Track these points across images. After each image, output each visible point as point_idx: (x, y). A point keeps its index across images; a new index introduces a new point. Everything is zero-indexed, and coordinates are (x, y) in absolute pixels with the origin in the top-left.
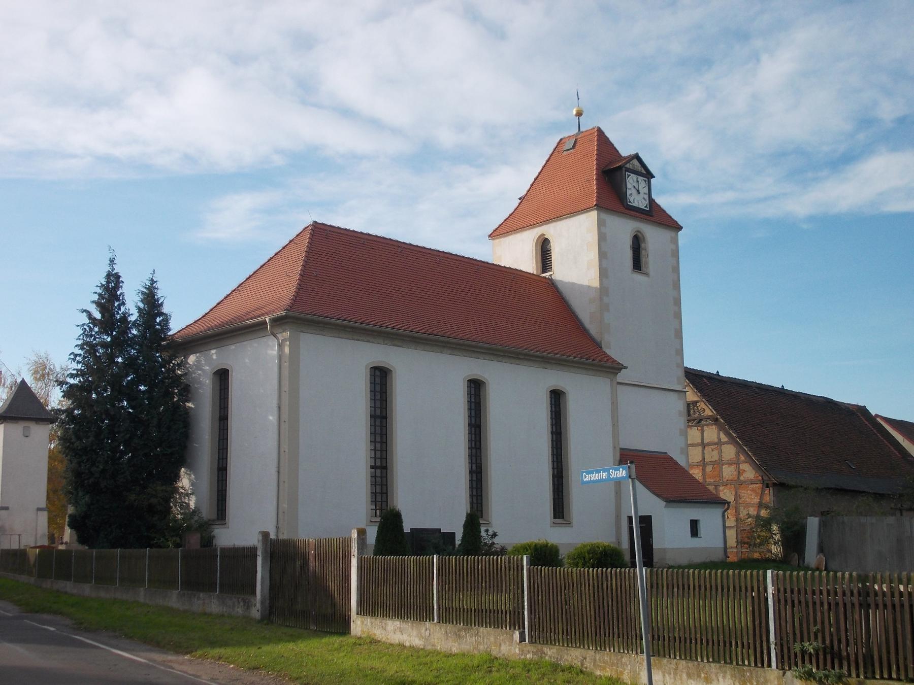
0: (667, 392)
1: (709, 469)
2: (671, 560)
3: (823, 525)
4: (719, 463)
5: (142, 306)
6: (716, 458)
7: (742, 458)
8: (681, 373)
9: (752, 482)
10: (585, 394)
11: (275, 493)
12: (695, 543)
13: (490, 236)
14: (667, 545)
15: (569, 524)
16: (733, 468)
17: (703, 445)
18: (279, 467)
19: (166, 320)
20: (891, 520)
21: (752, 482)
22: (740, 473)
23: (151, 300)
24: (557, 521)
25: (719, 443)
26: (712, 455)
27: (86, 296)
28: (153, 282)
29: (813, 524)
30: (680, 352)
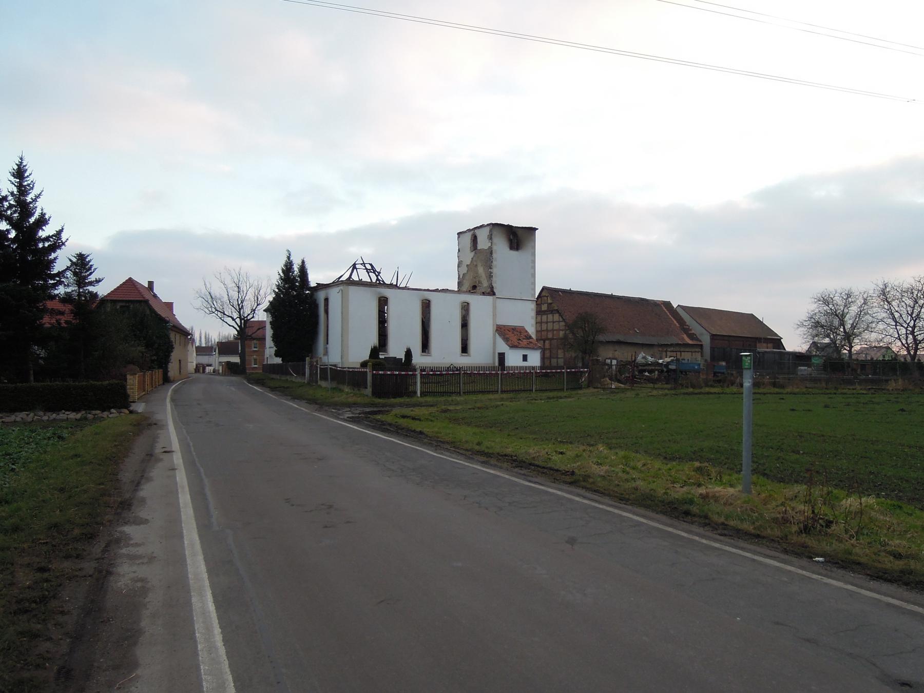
15: (469, 355)
28: (289, 258)
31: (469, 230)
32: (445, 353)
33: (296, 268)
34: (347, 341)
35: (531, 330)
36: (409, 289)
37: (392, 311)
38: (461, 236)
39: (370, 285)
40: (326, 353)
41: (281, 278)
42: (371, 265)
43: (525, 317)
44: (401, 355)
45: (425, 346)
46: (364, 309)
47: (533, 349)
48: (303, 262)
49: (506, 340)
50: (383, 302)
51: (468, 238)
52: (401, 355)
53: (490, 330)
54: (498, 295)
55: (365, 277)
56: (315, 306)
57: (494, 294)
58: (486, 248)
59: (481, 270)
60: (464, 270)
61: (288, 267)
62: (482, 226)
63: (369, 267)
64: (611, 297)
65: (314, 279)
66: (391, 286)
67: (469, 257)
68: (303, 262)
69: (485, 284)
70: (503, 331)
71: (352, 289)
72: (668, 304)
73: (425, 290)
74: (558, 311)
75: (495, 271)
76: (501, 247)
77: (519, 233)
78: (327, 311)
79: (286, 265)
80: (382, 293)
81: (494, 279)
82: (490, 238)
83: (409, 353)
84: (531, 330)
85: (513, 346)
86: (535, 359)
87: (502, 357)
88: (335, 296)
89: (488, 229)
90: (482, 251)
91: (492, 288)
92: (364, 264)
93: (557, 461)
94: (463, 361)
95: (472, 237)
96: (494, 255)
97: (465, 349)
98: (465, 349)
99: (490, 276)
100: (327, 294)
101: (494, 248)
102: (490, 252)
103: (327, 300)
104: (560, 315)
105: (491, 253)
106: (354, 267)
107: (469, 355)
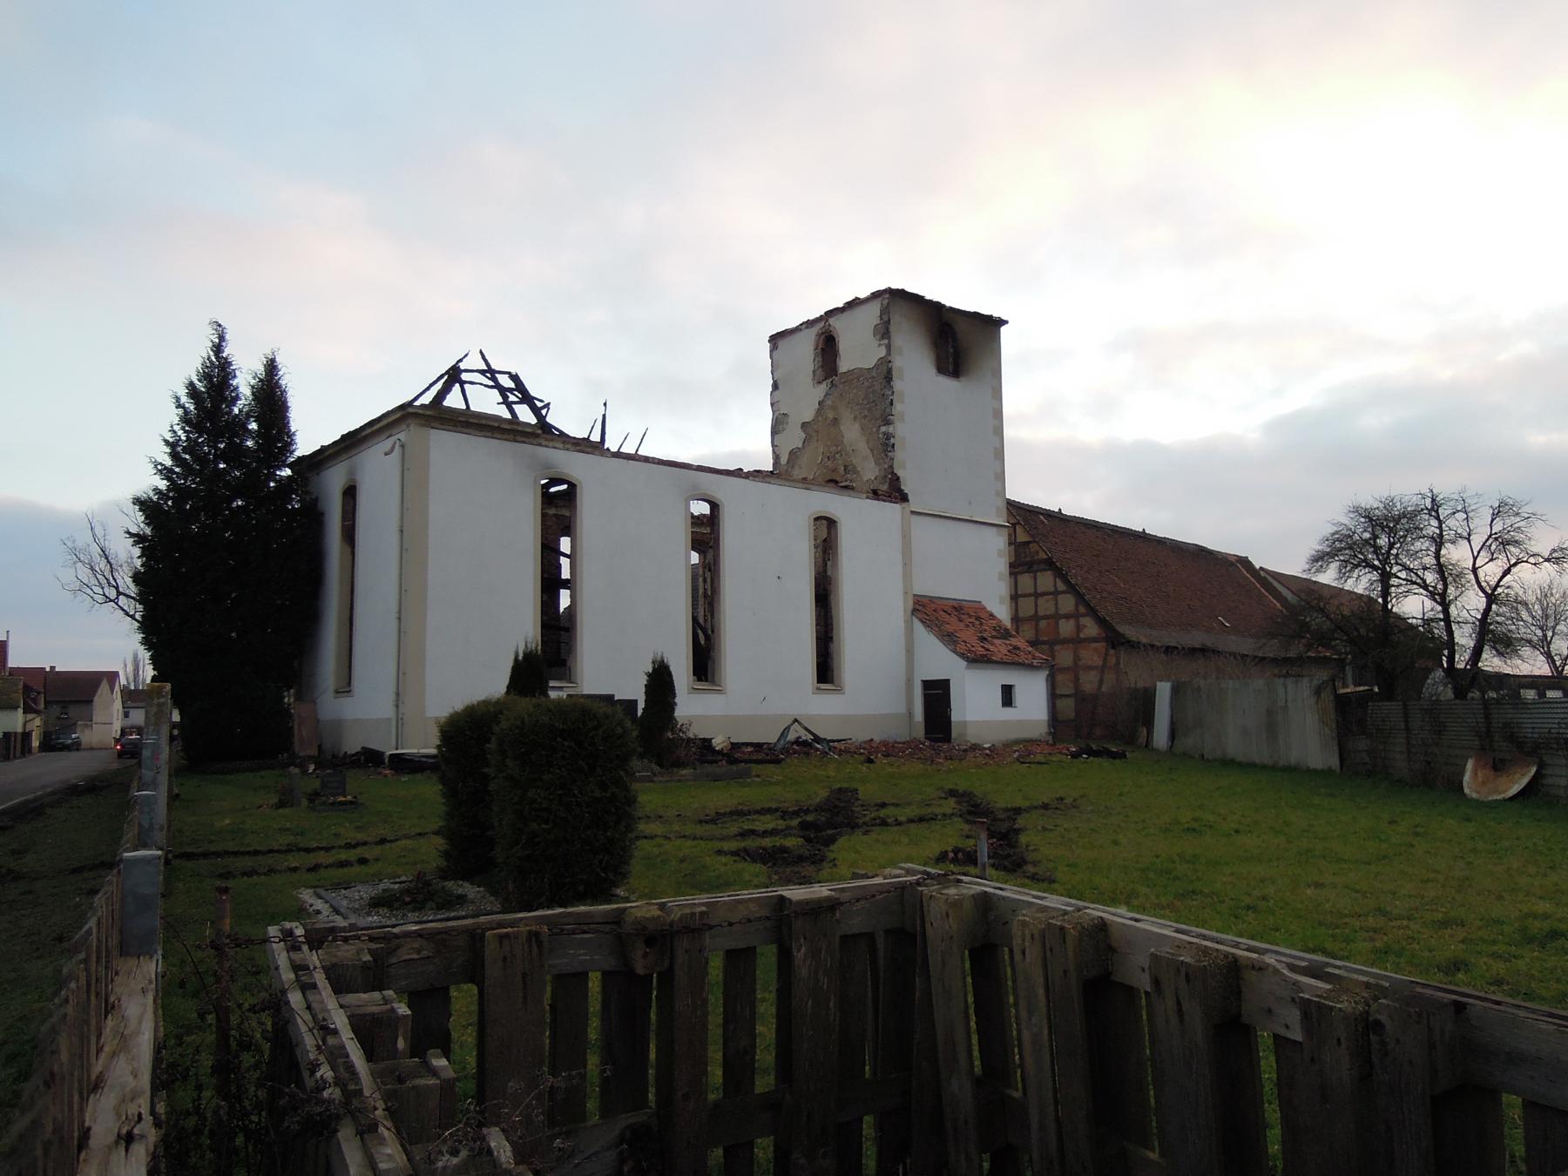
0: (948, 522)
1: (1043, 624)
2: (972, 737)
3: (1176, 691)
4: (1056, 617)
5: (200, 386)
6: (1052, 611)
7: (1082, 610)
8: (1003, 505)
9: (1095, 640)
10: (862, 521)
11: (395, 650)
12: (1009, 714)
13: (273, 361)
14: (970, 717)
15: (839, 690)
16: (1072, 622)
17: (1037, 595)
18: (400, 612)
19: (292, 443)
20: (1259, 683)
21: (1095, 640)
22: (1079, 628)
23: (271, 396)
24: (823, 686)
25: (1056, 593)
26: (1046, 606)
27: (189, 365)
28: (218, 348)
29: (1164, 690)
30: (1001, 477)
31: (809, 324)
32: (760, 688)
33: (244, 383)
34: (423, 645)
35: (1002, 612)
36: (647, 459)
37: (593, 548)
38: (781, 343)
39: (508, 430)
40: (345, 686)
41: (186, 419)
42: (515, 378)
43: (981, 574)
44: (633, 689)
45: (705, 664)
46: (485, 510)
47: (1030, 667)
48: (271, 367)
49: (949, 639)
50: (558, 510)
51: (805, 351)
52: (633, 689)
53: (896, 610)
54: (914, 505)
55: (486, 402)
56: (313, 515)
57: (904, 498)
58: (870, 363)
59: (852, 433)
60: (794, 438)
61: (218, 375)
62: (854, 304)
63: (506, 382)
64: (1142, 537)
65: (311, 431)
66: (583, 445)
67: (808, 398)
68: (271, 367)
69: (870, 471)
70: (933, 613)
71: (443, 444)
72: (1245, 562)
73: (700, 469)
74: (1050, 564)
75: (902, 430)
76: (914, 362)
77: (961, 326)
78: (349, 535)
79: (206, 376)
80: (559, 481)
81: (899, 455)
82: (884, 331)
83: (660, 679)
84: (1002, 612)
85: (978, 659)
86: (1033, 700)
87: (937, 695)
88: (377, 472)
89: (875, 309)
90: (856, 375)
91: (895, 480)
92: (490, 372)
93: (1041, 980)
94: (825, 712)
95: (824, 336)
96: (897, 384)
97: (826, 671)
98: (826, 671)
99: (886, 447)
100: (352, 472)
101: (898, 362)
102: (885, 373)
103: (350, 493)
104: (1060, 574)
105: (888, 377)
106: (454, 376)
107: (839, 690)
